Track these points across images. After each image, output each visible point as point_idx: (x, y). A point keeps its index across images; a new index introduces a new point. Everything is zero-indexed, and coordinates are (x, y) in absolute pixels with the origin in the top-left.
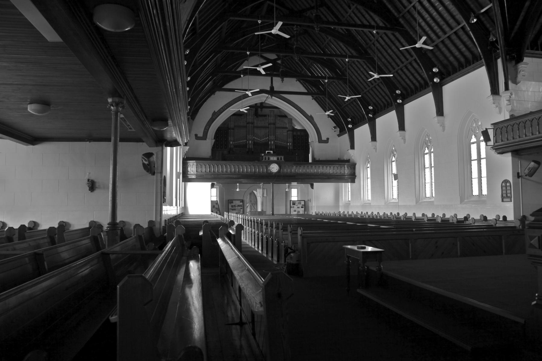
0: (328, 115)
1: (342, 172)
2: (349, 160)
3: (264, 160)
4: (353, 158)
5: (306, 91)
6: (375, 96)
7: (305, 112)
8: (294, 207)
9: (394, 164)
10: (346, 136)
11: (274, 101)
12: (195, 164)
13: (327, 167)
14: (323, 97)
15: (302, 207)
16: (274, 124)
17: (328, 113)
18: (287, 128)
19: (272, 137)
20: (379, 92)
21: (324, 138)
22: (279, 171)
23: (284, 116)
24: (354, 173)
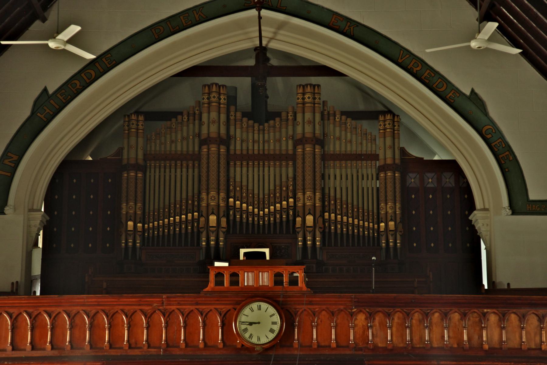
3: (212, 284)
16: (320, 142)
18: (375, 157)
19: (307, 198)
22: (284, 338)
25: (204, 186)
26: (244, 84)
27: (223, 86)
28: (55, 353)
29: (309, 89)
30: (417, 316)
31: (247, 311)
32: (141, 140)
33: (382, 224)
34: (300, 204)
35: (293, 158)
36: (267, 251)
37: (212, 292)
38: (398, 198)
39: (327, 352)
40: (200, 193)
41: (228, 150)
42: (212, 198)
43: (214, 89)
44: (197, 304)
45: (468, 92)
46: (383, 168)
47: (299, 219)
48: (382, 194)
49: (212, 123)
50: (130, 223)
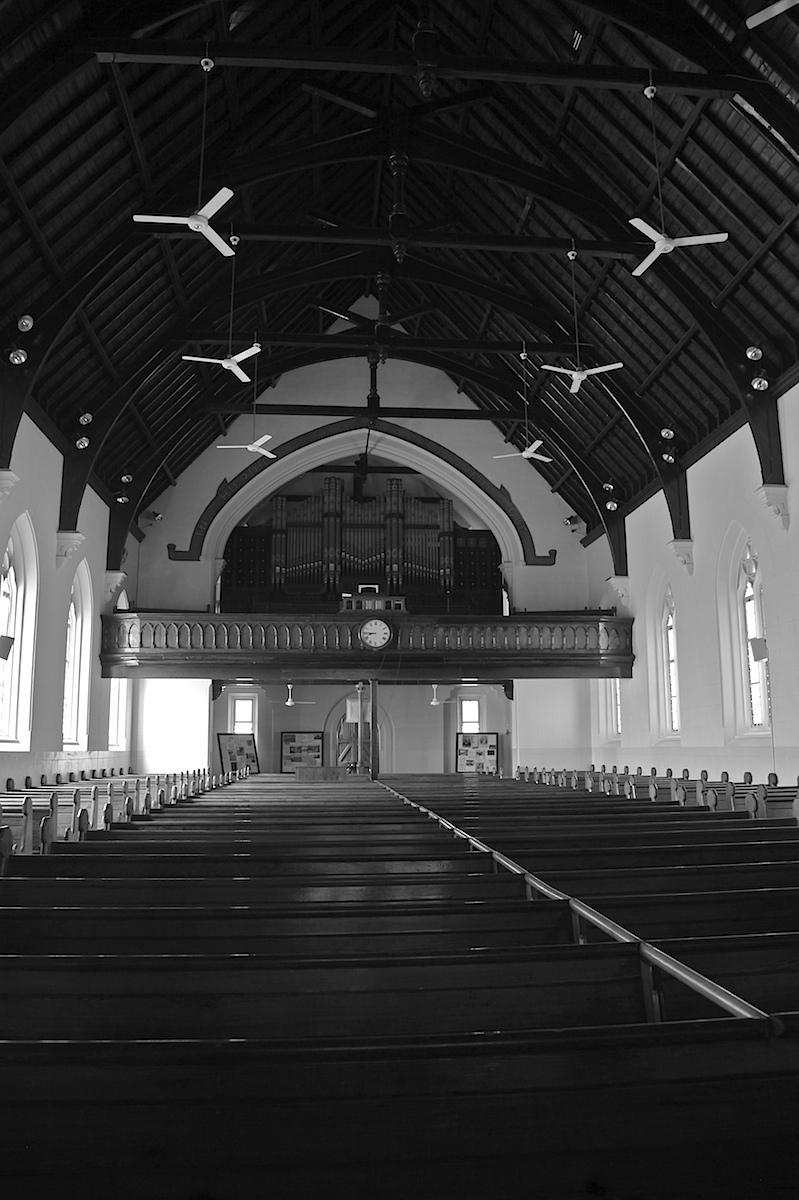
0: (531, 460)
1: (591, 645)
2: (614, 609)
3: (344, 609)
4: (624, 601)
5: (475, 407)
6: (680, 395)
7: (487, 474)
8: (466, 753)
9: (751, 607)
10: (603, 543)
11: (390, 449)
12: (137, 622)
13: (540, 630)
14: (512, 406)
15: (490, 753)
16: (402, 516)
17: (529, 453)
18: (438, 527)
19: (394, 553)
20: (691, 377)
21: (541, 551)
22: (392, 643)
23: (435, 498)
24: (630, 648)
25: (325, 542)
26: (348, 477)
27: (339, 479)
28: (244, 650)
29: (395, 482)
30: (476, 629)
31: (368, 625)
32: (284, 513)
33: (442, 571)
34: (388, 557)
35: (384, 526)
36: (376, 587)
37: (345, 614)
38: (452, 553)
39: (418, 652)
40: (323, 549)
41: (341, 521)
42: (331, 552)
43: (333, 480)
44: (334, 621)
45: (499, 487)
46: (442, 534)
47: (388, 567)
48: (441, 551)
49: (331, 503)
50: (278, 568)
